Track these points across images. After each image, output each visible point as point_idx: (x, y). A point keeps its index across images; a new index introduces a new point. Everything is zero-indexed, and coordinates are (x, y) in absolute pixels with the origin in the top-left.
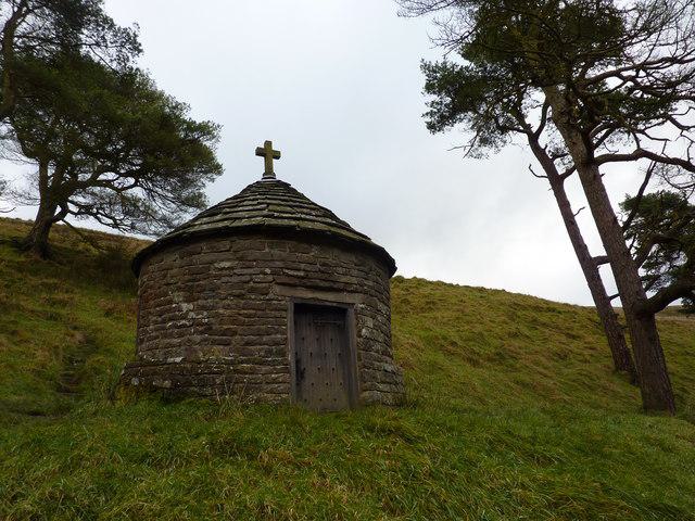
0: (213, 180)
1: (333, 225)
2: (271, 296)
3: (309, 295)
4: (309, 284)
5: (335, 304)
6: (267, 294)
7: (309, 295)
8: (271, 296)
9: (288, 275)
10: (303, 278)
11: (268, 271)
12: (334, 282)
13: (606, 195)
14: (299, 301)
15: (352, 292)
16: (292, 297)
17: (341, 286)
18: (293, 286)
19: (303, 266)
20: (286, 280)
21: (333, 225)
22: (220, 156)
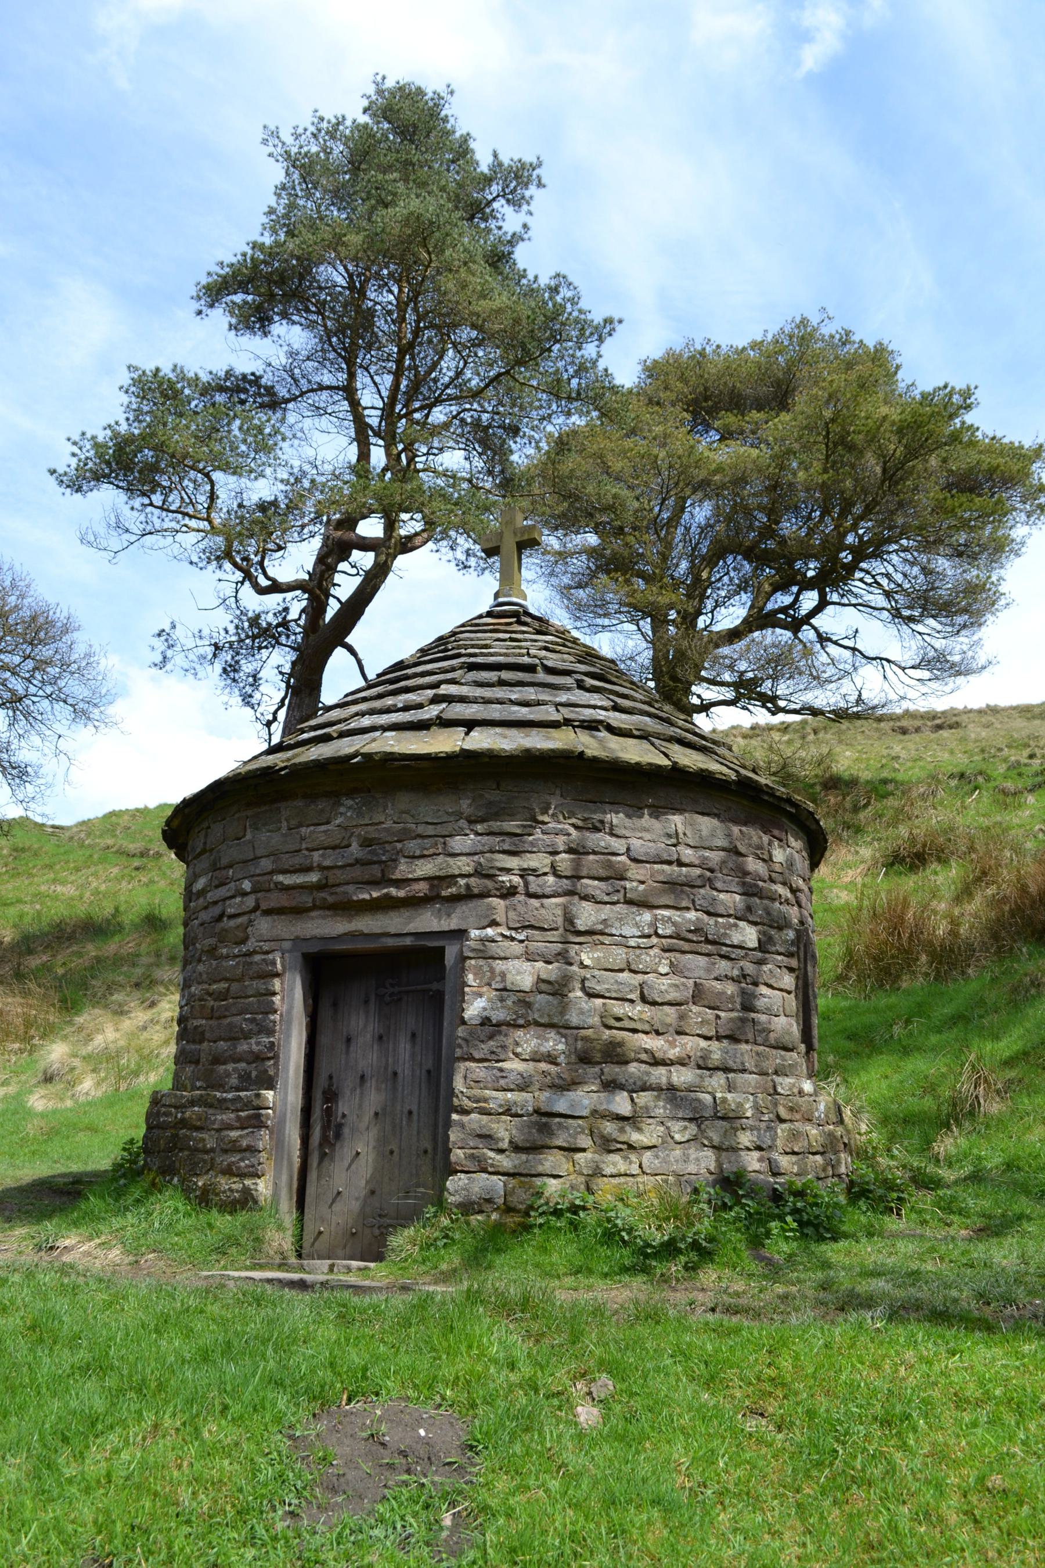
0: (209, 274)
1: (687, 731)
2: (251, 945)
3: (335, 927)
4: (331, 899)
5: (408, 941)
6: (244, 941)
7: (335, 927)
8: (251, 945)
9: (288, 888)
10: (320, 887)
11: (247, 885)
12: (399, 883)
13: (320, 691)
14: (313, 949)
15: (456, 899)
16: (297, 940)
17: (422, 888)
18: (298, 912)
19: (316, 856)
20: (276, 900)
21: (687, 731)
22: (225, 368)
